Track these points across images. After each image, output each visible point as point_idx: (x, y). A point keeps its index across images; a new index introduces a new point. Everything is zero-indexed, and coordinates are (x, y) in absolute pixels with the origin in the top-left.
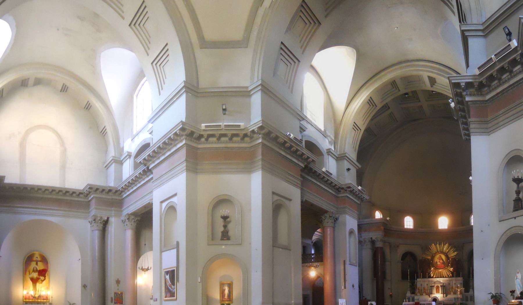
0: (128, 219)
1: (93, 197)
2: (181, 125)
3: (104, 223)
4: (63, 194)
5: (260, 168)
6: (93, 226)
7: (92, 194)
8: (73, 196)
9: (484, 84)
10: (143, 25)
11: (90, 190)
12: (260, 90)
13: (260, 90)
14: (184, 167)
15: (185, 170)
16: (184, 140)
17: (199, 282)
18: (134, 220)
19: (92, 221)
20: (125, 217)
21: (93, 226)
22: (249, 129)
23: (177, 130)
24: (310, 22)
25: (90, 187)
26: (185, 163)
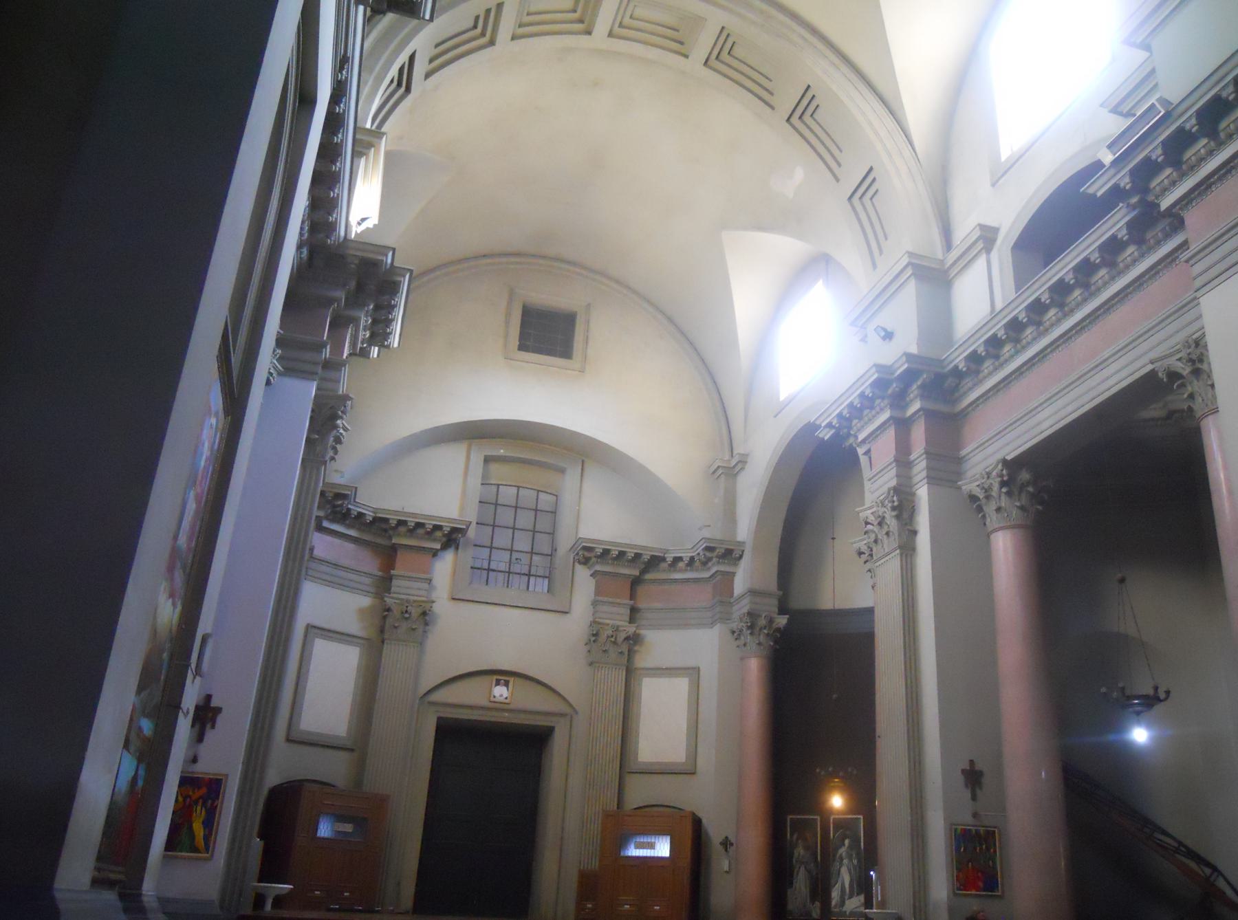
0: (749, 628)
1: (717, 572)
2: (874, 374)
3: (778, 635)
4: (670, 565)
5: (923, 470)
6: (745, 645)
7: (713, 565)
8: (678, 569)
9: (1194, 134)
10: (871, 199)
11: (709, 554)
12: (913, 277)
13: (913, 277)
14: (923, 470)
15: (925, 481)
16: (918, 399)
17: (727, 872)
18: (766, 631)
19: (741, 631)
20: (741, 621)
21: (745, 645)
22: (896, 371)
23: (865, 388)
24: (908, 140)
25: (708, 545)
26: (925, 461)
